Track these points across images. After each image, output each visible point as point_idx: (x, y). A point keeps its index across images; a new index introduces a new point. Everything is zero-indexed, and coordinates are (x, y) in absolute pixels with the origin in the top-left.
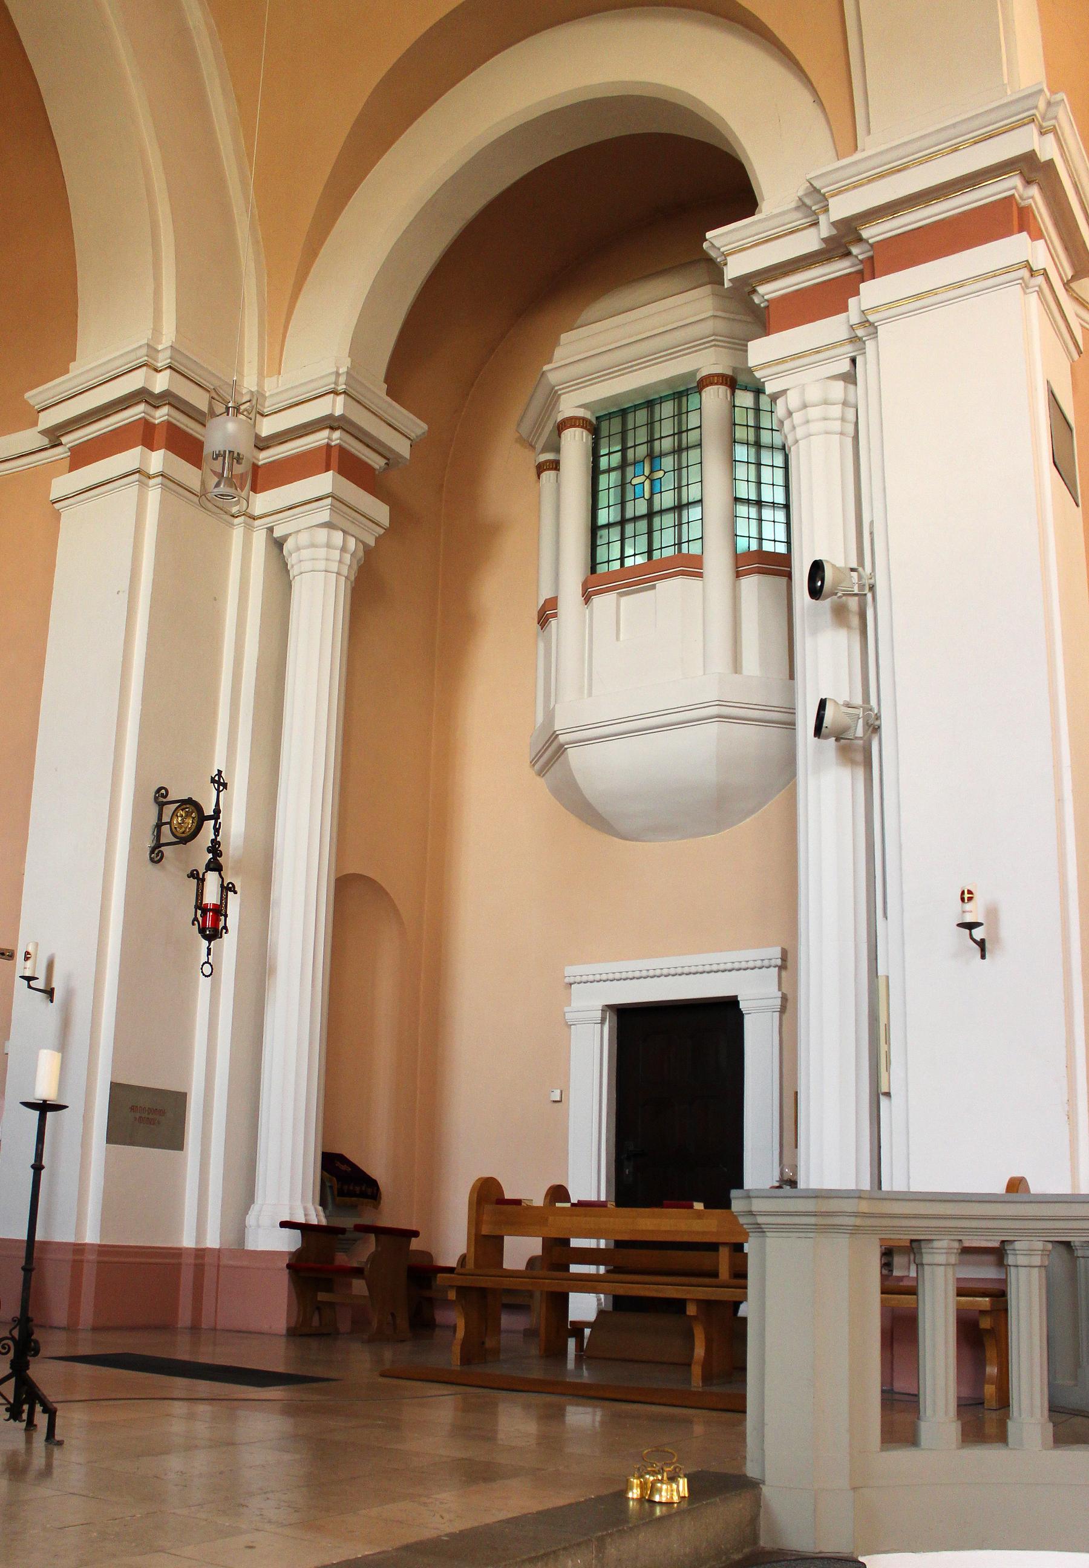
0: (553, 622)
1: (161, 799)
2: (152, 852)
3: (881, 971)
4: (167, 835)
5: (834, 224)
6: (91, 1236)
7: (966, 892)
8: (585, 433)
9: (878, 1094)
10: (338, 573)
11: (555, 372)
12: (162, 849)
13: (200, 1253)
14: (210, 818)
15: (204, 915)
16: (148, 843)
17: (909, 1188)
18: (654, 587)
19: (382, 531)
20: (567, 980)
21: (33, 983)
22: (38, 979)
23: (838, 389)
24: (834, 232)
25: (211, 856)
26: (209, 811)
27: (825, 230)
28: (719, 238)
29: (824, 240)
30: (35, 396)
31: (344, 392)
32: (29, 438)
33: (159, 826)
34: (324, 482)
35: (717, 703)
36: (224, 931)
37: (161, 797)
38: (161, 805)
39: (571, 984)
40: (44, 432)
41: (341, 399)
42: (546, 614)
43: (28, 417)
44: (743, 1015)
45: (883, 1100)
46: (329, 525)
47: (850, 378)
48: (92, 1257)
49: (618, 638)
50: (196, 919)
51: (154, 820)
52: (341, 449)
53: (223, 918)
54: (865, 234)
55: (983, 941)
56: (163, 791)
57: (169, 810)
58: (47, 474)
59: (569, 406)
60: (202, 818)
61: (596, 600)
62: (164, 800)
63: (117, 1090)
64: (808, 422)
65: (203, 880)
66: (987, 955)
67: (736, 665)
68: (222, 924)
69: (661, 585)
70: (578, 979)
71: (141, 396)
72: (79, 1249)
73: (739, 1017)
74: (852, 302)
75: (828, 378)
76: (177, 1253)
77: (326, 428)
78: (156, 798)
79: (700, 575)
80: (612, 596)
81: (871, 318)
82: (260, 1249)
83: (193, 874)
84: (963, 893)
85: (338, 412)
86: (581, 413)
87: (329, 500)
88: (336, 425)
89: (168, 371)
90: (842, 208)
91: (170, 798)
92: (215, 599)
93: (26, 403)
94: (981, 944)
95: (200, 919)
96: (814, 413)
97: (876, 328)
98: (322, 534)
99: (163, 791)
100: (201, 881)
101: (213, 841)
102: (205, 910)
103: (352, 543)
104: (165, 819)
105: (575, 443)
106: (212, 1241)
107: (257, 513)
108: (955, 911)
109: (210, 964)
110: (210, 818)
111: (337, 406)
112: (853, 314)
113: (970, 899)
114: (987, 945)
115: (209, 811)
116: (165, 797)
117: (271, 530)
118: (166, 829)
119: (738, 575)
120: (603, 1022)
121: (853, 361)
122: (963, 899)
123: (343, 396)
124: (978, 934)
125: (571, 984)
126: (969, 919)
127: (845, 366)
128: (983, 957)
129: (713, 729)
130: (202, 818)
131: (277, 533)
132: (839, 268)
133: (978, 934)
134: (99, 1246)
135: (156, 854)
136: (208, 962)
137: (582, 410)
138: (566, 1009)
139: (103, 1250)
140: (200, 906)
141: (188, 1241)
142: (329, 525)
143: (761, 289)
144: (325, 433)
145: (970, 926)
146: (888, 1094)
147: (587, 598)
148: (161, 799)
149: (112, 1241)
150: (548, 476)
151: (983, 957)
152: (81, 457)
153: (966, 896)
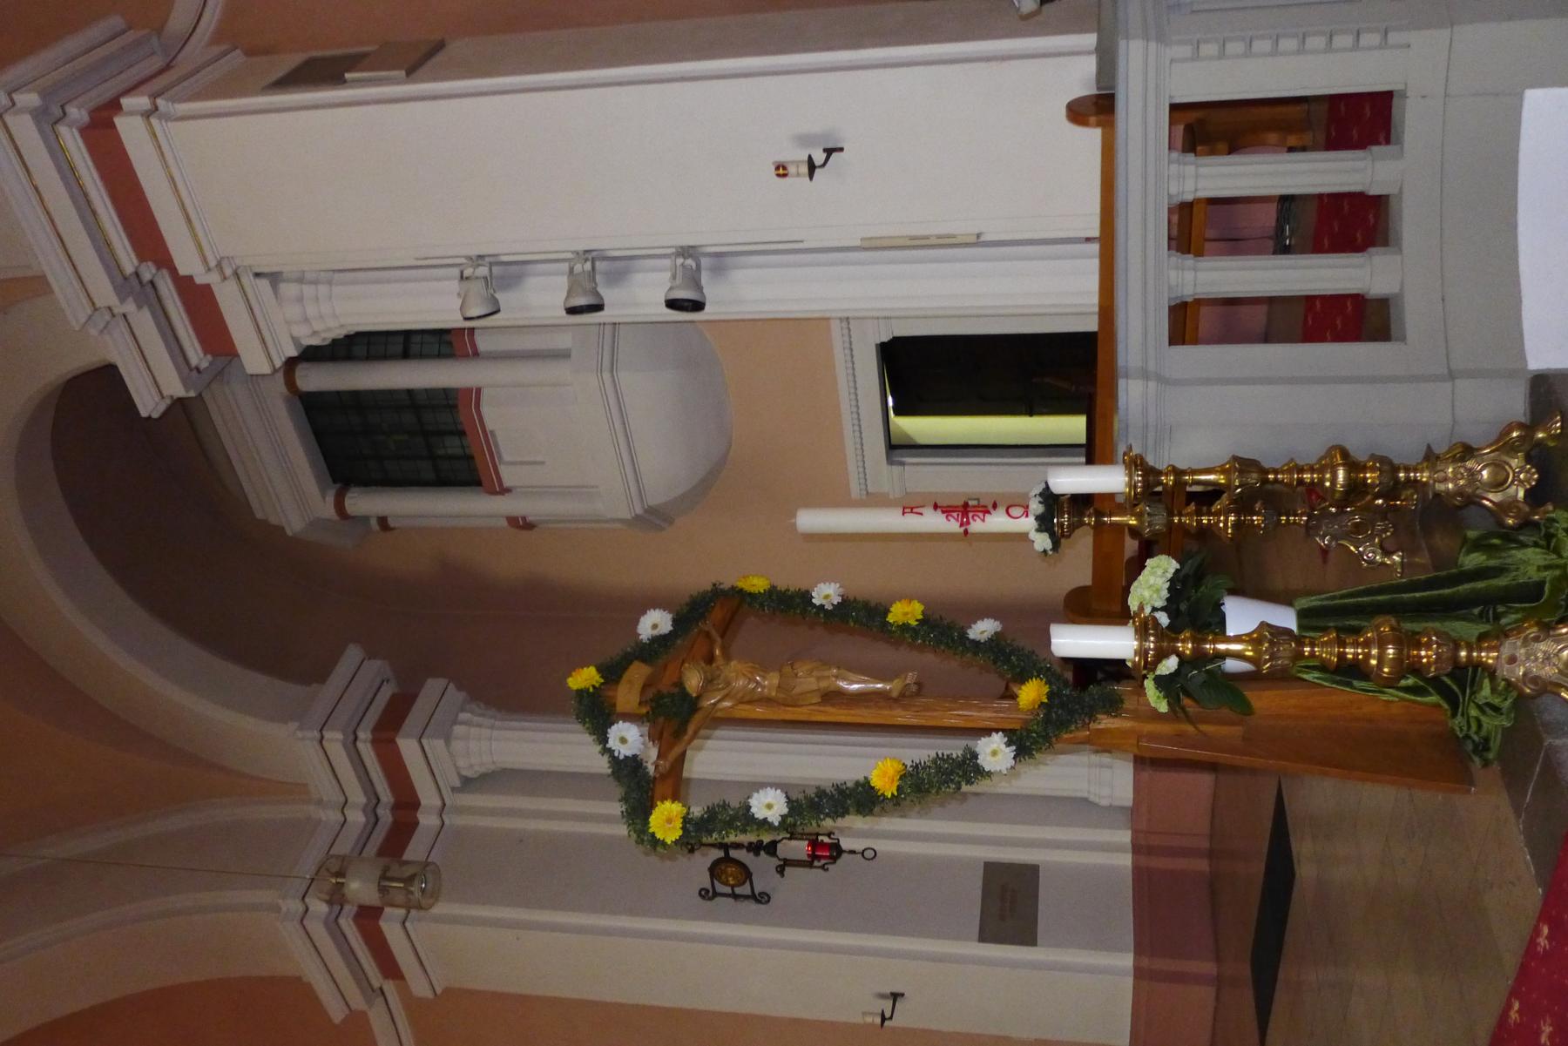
0: (530, 519)
1: (711, 894)
2: (760, 902)
3: (858, 243)
4: (745, 890)
5: (122, 300)
6: (1127, 961)
7: (778, 172)
8: (349, 495)
9: (978, 242)
10: (490, 739)
11: (294, 523)
12: (757, 892)
13: (1137, 849)
14: (727, 853)
15: (819, 858)
16: (752, 906)
17: (1094, 313)
18: (492, 432)
19: (451, 686)
20: (864, 497)
21: (887, 1015)
22: (883, 1011)
23: (289, 290)
24: (131, 299)
25: (762, 853)
26: (720, 854)
27: (130, 307)
28: (148, 404)
29: (140, 307)
30: (337, 1013)
31: (321, 730)
32: (377, 1019)
33: (735, 896)
34: (407, 747)
35: (599, 375)
36: (832, 836)
37: (705, 894)
38: (716, 894)
39: (867, 493)
40: (369, 1002)
41: (328, 735)
42: (521, 524)
43: (358, 1021)
44: (894, 338)
45: (982, 239)
46: (448, 739)
47: (275, 278)
48: (1145, 962)
49: (542, 463)
50: (823, 867)
51: (731, 900)
52: (375, 730)
53: (820, 838)
54: (129, 269)
55: (825, 150)
56: (703, 893)
57: (720, 888)
58: (410, 1002)
59: (327, 510)
60: (727, 859)
61: (507, 483)
62: (711, 891)
63: (984, 937)
64: (321, 317)
65: (785, 860)
66: (839, 146)
67: (563, 355)
68: (826, 840)
69: (489, 426)
70: (863, 487)
71: (333, 925)
72: (1139, 973)
73: (896, 341)
74: (199, 280)
75: (277, 298)
76: (1138, 872)
77: (355, 746)
78: (711, 899)
79: (479, 391)
80: (503, 469)
81: (213, 263)
82: (1132, 796)
83: (781, 870)
84: (778, 175)
85: (340, 736)
86: (330, 499)
87: (424, 741)
88: (352, 737)
89: (307, 900)
90: (104, 292)
91: (708, 886)
92: (521, 841)
93: (344, 1021)
94: (829, 152)
95: (823, 862)
96: (311, 311)
97: (222, 258)
98: (457, 745)
99: (703, 893)
100: (787, 863)
101: (748, 851)
102: (814, 857)
103: (463, 716)
104: (728, 890)
105: (364, 503)
106: (1125, 837)
107: (439, 803)
108: (798, 182)
109: (863, 851)
110: (727, 853)
111: (334, 739)
112: (212, 279)
113: (784, 168)
114: (830, 146)
115: (720, 854)
116: (707, 891)
117: (454, 789)
118: (738, 890)
119: (476, 354)
120: (903, 464)
121: (257, 275)
122: (785, 175)
123: (324, 732)
124: (819, 157)
125: (867, 493)
126: (805, 169)
127: (264, 284)
128: (841, 150)
129: (624, 377)
130: (727, 859)
131: (457, 783)
132: (167, 288)
133: (819, 157)
134: (1135, 953)
135: (762, 898)
136: (863, 853)
137: (327, 499)
138: (891, 497)
139: (1139, 951)
140: (808, 864)
141: (1126, 860)
142: (448, 739)
143: (194, 361)
144: (360, 745)
145: (812, 167)
146: (978, 236)
147: (505, 491)
148: (711, 894)
149: (1130, 939)
150: (391, 522)
151: (841, 150)
152: (390, 968)
153: (781, 171)
